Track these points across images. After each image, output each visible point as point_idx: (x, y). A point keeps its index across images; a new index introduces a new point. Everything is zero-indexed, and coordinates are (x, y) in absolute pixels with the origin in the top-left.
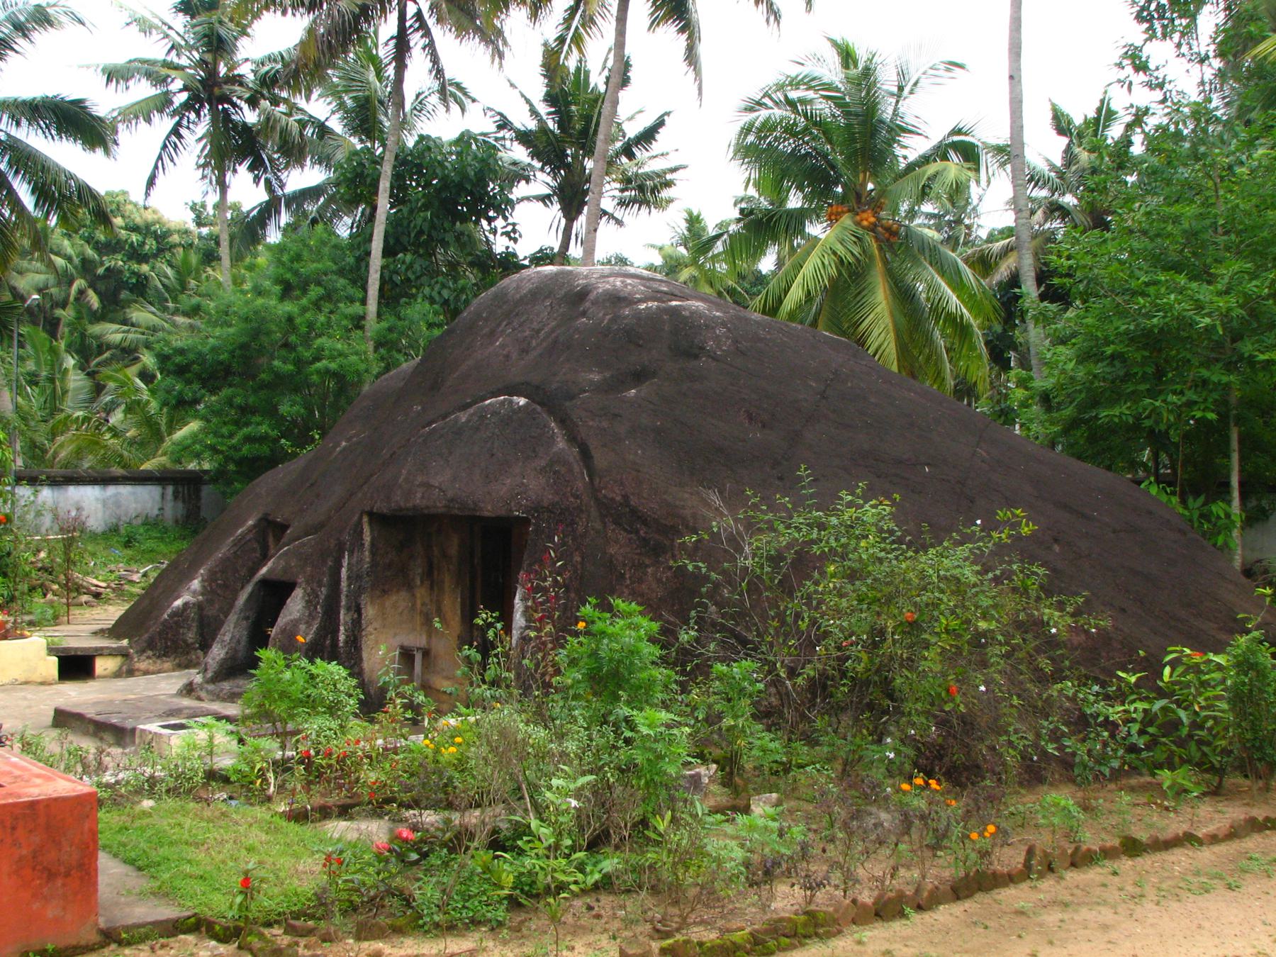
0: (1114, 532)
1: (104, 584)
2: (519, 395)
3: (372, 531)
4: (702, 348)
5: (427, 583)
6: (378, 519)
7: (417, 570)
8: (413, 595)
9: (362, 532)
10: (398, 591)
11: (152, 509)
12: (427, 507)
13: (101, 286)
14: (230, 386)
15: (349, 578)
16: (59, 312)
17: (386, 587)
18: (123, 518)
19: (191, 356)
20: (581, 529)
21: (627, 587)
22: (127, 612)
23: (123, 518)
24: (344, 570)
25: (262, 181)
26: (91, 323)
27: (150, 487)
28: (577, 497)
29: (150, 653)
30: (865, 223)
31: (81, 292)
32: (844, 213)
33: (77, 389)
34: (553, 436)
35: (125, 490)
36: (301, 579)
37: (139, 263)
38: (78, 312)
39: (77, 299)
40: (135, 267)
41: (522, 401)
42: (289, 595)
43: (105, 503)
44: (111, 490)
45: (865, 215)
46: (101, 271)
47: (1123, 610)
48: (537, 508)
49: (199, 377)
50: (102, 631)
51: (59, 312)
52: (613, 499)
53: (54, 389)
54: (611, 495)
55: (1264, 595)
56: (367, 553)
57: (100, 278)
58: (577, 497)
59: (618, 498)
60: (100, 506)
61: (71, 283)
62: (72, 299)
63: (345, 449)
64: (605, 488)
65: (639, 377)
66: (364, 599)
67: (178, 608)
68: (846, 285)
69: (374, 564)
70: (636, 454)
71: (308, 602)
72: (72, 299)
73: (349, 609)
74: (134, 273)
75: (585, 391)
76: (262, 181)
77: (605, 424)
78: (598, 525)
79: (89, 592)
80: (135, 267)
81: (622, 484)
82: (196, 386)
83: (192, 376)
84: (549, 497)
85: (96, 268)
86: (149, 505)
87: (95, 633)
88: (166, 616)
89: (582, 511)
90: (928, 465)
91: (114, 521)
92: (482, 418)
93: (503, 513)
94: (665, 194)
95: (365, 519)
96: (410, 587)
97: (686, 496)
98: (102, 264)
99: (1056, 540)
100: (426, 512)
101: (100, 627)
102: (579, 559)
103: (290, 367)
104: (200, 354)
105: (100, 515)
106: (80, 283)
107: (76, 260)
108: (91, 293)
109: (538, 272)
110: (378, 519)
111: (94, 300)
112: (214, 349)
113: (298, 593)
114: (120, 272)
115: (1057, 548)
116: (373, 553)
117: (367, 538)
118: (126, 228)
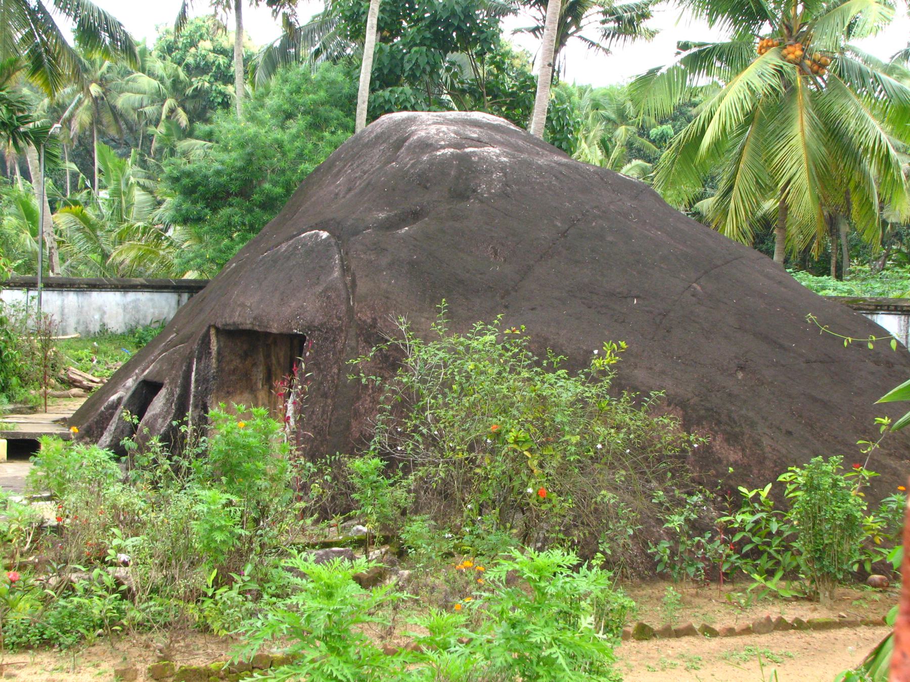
0: (808, 362)
1: (97, 380)
2: (324, 229)
3: (218, 341)
4: (474, 191)
5: (266, 387)
6: (222, 332)
7: (259, 375)
8: (256, 396)
9: (209, 342)
10: (241, 393)
11: (169, 313)
12: (241, 324)
13: (189, 105)
14: (231, 205)
15: (196, 381)
16: (151, 129)
17: (231, 389)
18: (142, 322)
19: (198, 178)
20: (339, 346)
21: (369, 395)
22: (86, 403)
23: (142, 322)
24: (193, 374)
25: (280, 15)
26: (180, 139)
27: (166, 294)
28: (340, 319)
29: (88, 439)
30: (791, 57)
31: (172, 111)
32: (773, 46)
33: (140, 202)
34: (332, 268)
35: (143, 297)
36: (167, 381)
37: (225, 83)
38: (168, 129)
39: (168, 117)
40: (221, 87)
41: (324, 235)
42: (156, 394)
43: (125, 308)
44: (131, 296)
45: (790, 49)
46: (189, 91)
47: (789, 433)
48: (310, 327)
49: (203, 197)
50: (64, 419)
51: (151, 129)
52: (365, 321)
53: (121, 202)
54: (364, 318)
55: (881, 424)
56: (214, 360)
57: (187, 98)
58: (340, 319)
59: (369, 321)
60: (121, 311)
61: (163, 101)
62: (163, 117)
63: (235, 267)
64: (361, 312)
65: (415, 216)
66: (210, 399)
67: (113, 402)
68: (765, 117)
69: (220, 369)
70: (390, 284)
71: (168, 400)
72: (163, 117)
73: (196, 406)
74: (220, 93)
75: (368, 228)
76: (280, 15)
77: (373, 257)
78: (353, 343)
79: (81, 386)
80: (221, 87)
81: (373, 309)
82: (199, 206)
83: (204, 198)
84: (319, 319)
85: (184, 88)
86: (166, 310)
87: (55, 422)
88: (103, 408)
89: (342, 331)
90: (637, 297)
91: (133, 324)
92: (296, 248)
93: (285, 330)
94: (645, 24)
95: (213, 332)
96: (253, 390)
97: (423, 320)
98: (191, 84)
99: (741, 368)
100: (240, 327)
101: (62, 416)
102: (336, 371)
103: (279, 190)
104: (206, 177)
105: (120, 318)
106: (170, 102)
107: (168, 82)
108: (180, 111)
109: (391, 118)
110: (222, 332)
111: (183, 118)
112: (218, 173)
113: (163, 392)
114: (207, 92)
115: (740, 375)
116: (219, 361)
117: (214, 347)
118: (214, 51)
